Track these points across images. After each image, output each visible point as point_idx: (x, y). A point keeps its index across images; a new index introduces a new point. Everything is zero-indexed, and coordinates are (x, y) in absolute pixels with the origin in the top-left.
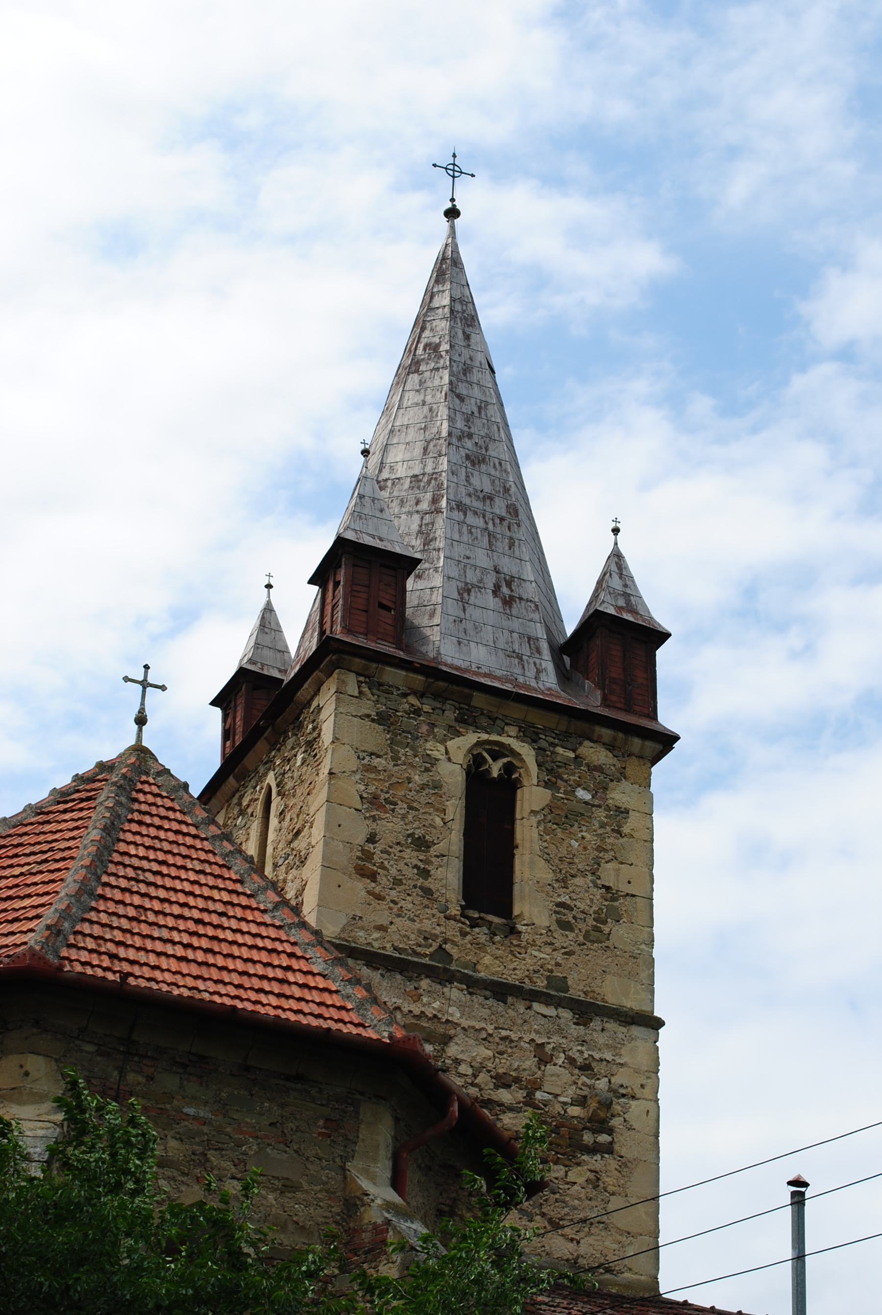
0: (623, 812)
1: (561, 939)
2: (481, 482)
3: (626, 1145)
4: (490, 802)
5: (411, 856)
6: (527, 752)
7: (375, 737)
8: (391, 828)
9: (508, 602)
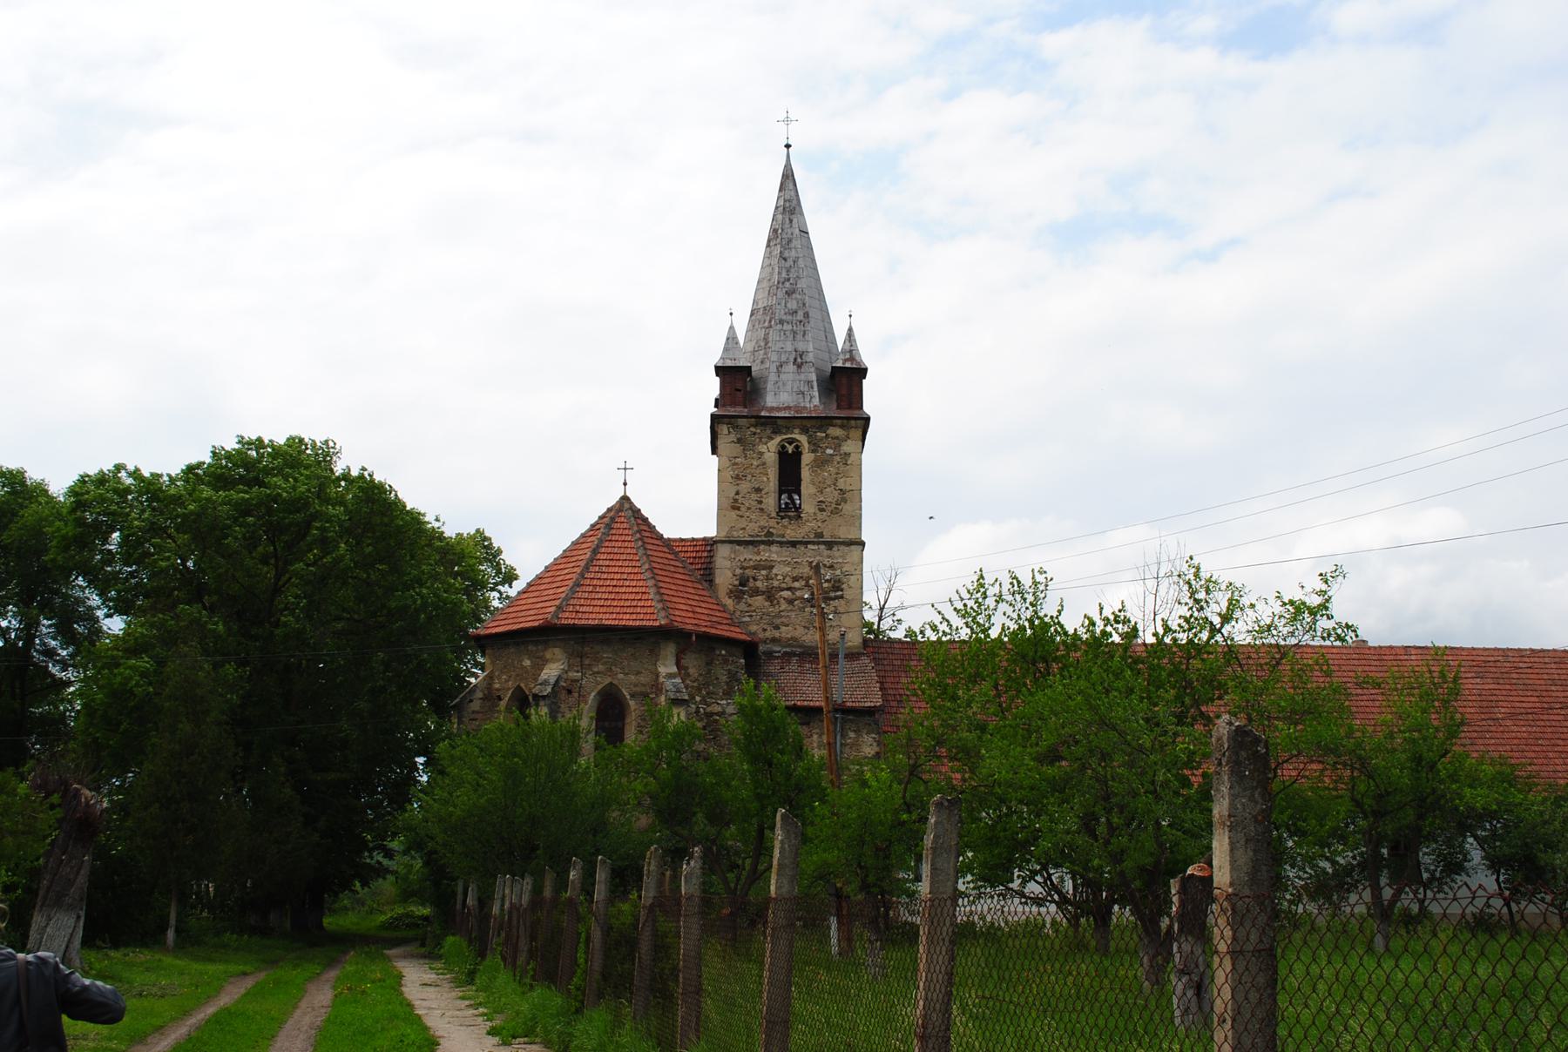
0: (848, 455)
1: (820, 516)
2: (792, 305)
3: (848, 594)
4: (789, 466)
5: (754, 496)
6: (803, 439)
7: (738, 448)
8: (745, 486)
9: (799, 366)
